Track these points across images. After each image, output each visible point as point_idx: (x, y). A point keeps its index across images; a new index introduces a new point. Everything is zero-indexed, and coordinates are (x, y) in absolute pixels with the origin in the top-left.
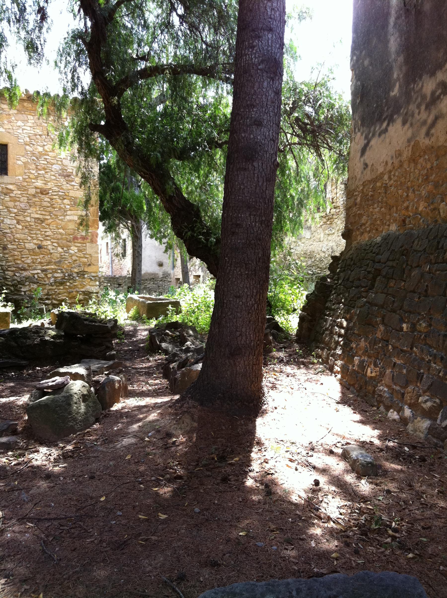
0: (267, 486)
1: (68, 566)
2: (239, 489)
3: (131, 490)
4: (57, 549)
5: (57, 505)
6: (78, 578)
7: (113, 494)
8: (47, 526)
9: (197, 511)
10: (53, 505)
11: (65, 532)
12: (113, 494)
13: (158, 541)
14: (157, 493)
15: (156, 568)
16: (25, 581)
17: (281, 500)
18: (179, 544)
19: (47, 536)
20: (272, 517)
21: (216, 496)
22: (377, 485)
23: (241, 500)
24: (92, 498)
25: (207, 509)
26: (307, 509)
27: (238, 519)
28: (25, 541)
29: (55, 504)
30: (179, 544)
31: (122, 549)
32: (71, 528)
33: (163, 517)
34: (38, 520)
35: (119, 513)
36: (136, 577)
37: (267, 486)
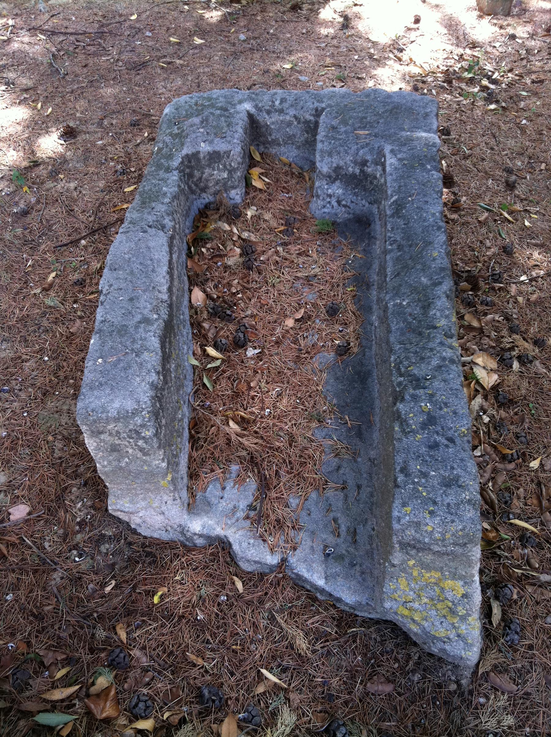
0: (346, 18)
1: (74, 81)
2: (308, 20)
3: (171, 10)
4: (67, 64)
5: (79, 20)
6: (82, 93)
7: (148, 13)
8: (61, 39)
9: (242, 39)
10: (74, 19)
11: (80, 48)
12: (148, 13)
13: (182, 65)
14: (202, 17)
15: (170, 91)
16: (26, 90)
17: (357, 36)
18: (206, 70)
19: (59, 51)
20: (336, 53)
21: (274, 26)
22: (501, 27)
23: (304, 31)
24: (121, 15)
25: (256, 38)
26: (388, 49)
27: (290, 53)
28: (34, 53)
29: (76, 18)
30: (206, 70)
31: (139, 70)
32: (89, 45)
33: (198, 41)
34: (52, 33)
35: (148, 34)
36: (144, 97)
37: (346, 18)
